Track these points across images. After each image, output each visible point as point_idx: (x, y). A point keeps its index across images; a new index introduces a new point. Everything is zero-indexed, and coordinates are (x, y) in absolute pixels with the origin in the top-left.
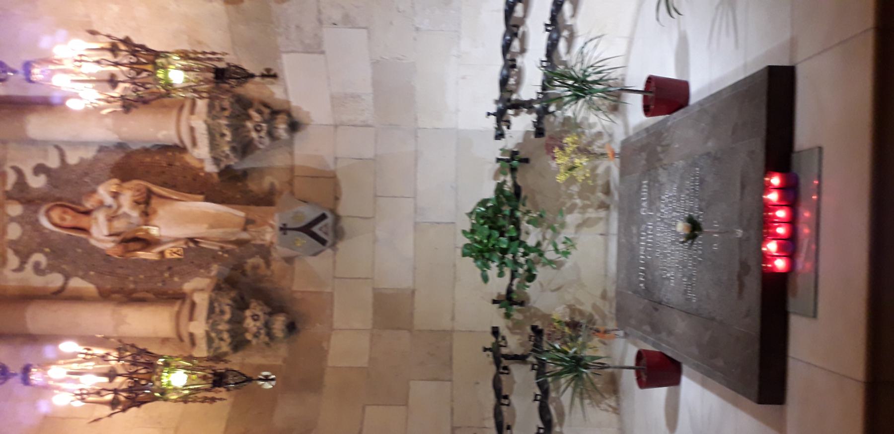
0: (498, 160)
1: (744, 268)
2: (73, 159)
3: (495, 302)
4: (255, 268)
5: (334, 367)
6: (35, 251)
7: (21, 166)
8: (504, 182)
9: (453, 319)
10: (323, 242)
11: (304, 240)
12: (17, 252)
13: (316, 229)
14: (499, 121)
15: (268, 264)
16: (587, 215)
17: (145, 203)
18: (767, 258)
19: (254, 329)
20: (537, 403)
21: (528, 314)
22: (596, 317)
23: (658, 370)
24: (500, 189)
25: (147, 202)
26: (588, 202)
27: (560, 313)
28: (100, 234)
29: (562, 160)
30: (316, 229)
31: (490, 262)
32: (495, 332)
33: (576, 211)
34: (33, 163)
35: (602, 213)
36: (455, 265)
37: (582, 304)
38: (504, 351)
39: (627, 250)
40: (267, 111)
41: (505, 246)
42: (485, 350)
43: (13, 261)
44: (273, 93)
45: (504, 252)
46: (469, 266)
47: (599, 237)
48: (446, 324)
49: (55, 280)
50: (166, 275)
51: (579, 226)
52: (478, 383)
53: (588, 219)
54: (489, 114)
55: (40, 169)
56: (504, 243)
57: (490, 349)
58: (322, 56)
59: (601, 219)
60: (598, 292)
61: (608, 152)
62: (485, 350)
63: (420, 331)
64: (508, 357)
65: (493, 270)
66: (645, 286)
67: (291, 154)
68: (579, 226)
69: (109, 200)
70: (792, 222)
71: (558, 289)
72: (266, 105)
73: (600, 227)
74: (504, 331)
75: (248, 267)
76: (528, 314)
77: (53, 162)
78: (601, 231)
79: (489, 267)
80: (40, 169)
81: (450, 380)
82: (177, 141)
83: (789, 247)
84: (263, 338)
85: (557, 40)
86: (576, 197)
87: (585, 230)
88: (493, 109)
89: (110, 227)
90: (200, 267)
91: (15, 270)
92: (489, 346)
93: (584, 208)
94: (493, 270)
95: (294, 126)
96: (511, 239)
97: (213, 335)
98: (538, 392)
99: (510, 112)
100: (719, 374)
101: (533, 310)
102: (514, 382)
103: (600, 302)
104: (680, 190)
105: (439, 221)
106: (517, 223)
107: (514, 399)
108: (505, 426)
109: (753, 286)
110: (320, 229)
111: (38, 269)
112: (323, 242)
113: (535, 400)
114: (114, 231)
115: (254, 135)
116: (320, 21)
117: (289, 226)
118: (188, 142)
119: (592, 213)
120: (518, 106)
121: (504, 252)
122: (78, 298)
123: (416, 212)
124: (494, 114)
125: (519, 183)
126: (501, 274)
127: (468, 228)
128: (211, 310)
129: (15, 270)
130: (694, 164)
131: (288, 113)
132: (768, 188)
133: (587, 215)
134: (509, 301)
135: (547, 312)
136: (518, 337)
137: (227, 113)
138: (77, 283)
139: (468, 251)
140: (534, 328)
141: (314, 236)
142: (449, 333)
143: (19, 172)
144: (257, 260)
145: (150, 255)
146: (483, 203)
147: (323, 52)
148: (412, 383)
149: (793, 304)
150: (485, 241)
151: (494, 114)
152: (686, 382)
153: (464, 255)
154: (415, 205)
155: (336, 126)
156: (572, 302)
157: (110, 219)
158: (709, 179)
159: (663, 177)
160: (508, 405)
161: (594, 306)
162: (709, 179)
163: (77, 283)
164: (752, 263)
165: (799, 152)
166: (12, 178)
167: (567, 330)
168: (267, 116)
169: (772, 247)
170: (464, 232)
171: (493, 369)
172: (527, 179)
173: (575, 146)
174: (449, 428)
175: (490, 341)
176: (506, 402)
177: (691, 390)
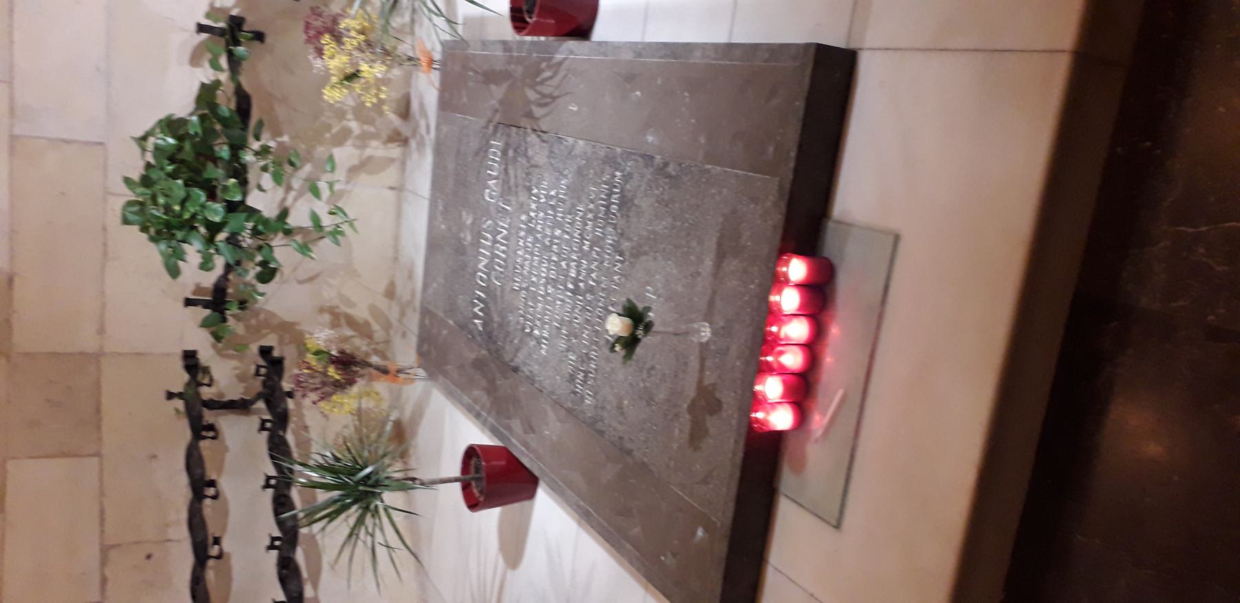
0: (201, 28)
1: (706, 403)
3: (189, 302)
8: (217, 84)
9: (101, 331)
16: (368, 152)
18: (758, 401)
21: (253, 322)
22: (376, 327)
23: (496, 479)
24: (207, 94)
26: (372, 129)
27: (321, 336)
29: (336, 61)
31: (185, 246)
32: (191, 360)
33: (349, 142)
35: (395, 151)
36: (104, 229)
37: (352, 305)
38: (206, 393)
39: (448, 248)
41: (217, 219)
45: (214, 228)
46: (140, 251)
47: (390, 194)
48: (87, 341)
51: (354, 171)
52: (154, 457)
53: (370, 158)
56: (216, 212)
57: (180, 395)
59: (392, 160)
60: (382, 286)
61: (419, 54)
63: (27, 354)
64: (212, 405)
65: (193, 252)
66: (484, 325)
68: (354, 171)
70: (812, 348)
71: (311, 279)
73: (390, 175)
74: (206, 355)
76: (253, 322)
78: (392, 181)
79: (180, 255)
81: (98, 454)
83: (801, 390)
86: (350, 116)
87: (363, 177)
92: (178, 388)
93: (364, 139)
94: (193, 252)
96: (232, 207)
100: (628, 546)
101: (262, 316)
102: (226, 449)
103: (382, 303)
104: (576, 192)
105: (66, 136)
106: (240, 173)
107: (226, 484)
108: (211, 540)
109: (725, 448)
113: (267, 486)
119: (376, 149)
121: (214, 228)
123: (12, 111)
125: (247, 87)
126: (206, 265)
127: (136, 176)
130: (611, 162)
132: (780, 282)
133: (368, 152)
134: (217, 303)
135: (288, 317)
136: (234, 363)
139: (137, 214)
140: (265, 352)
142: (96, 357)
146: (171, 125)
148: (10, 465)
149: (787, 480)
150: (177, 208)
152: (544, 500)
153: (126, 222)
154: (12, 99)
156: (336, 302)
158: (645, 203)
159: (538, 152)
160: (215, 497)
161: (373, 310)
162: (645, 203)
164: (728, 398)
165: (839, 222)
167: (332, 371)
169: (772, 387)
170: (127, 181)
171: (185, 433)
172: (261, 72)
173: (362, 37)
174: (95, 552)
175: (179, 379)
177: (548, 513)
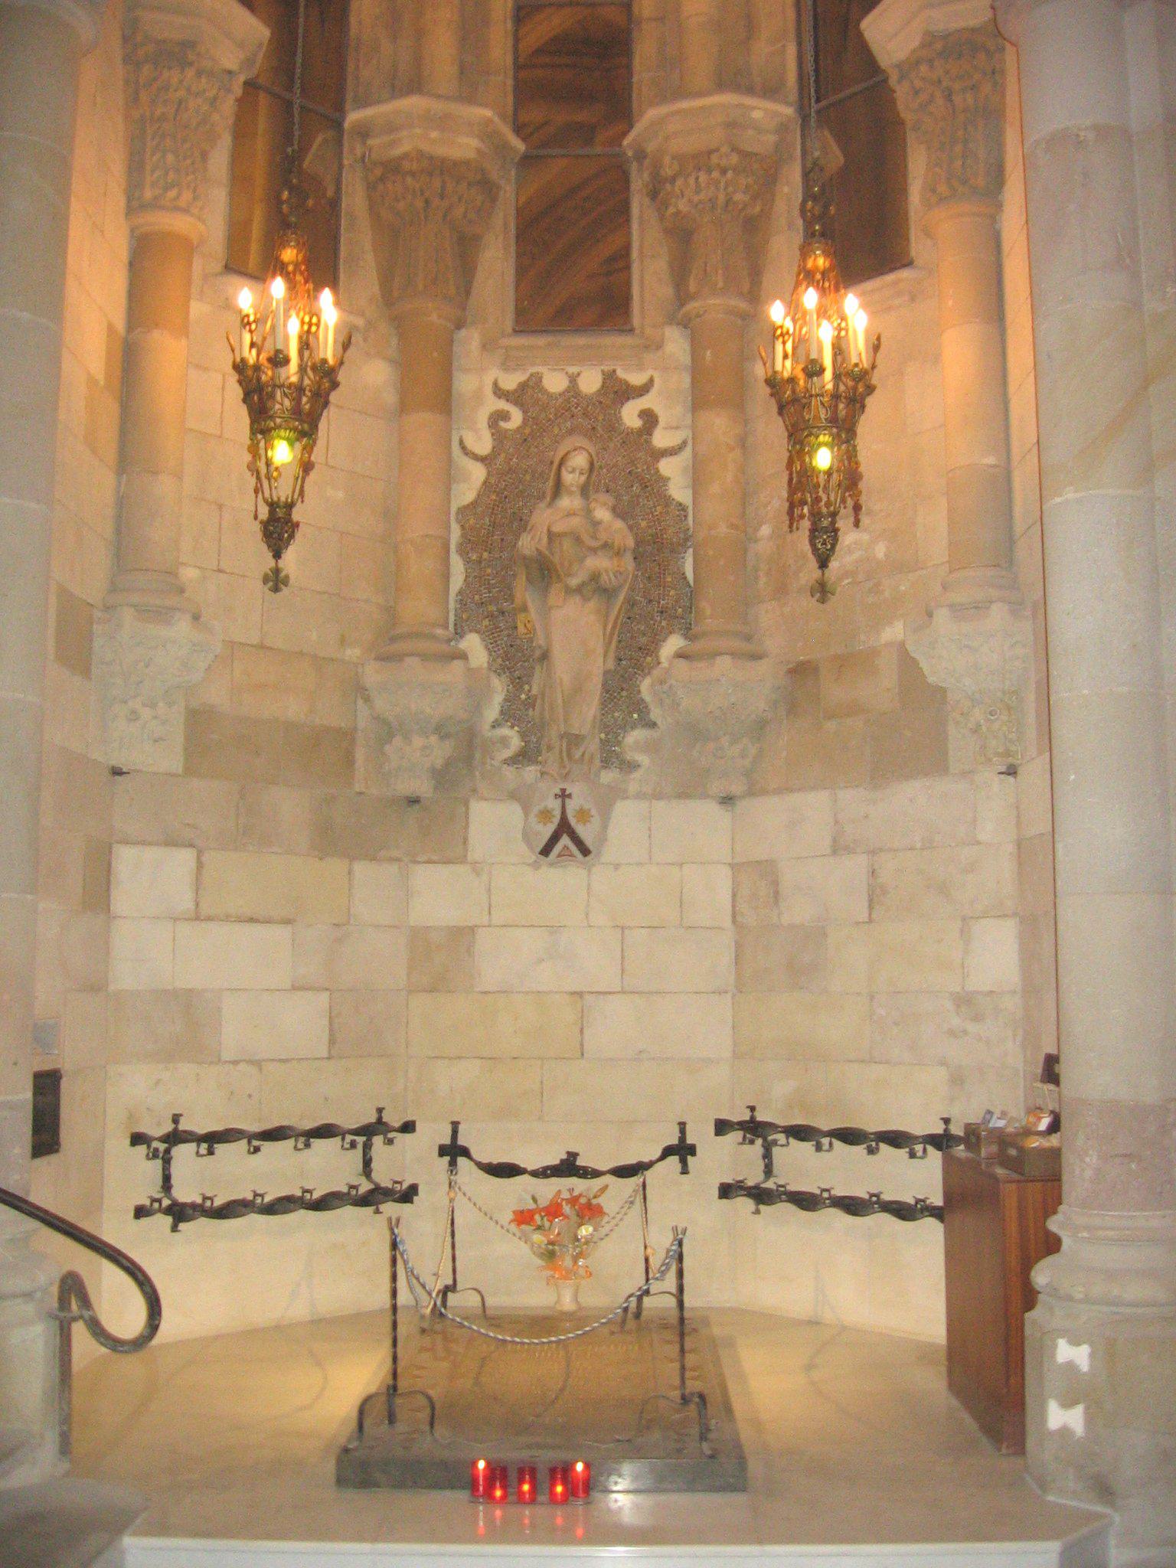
6: (525, 412)
12: (523, 386)
13: (565, 840)
17: (597, 588)
20: (867, 1197)
30: (565, 840)
34: (658, 410)
42: (380, 1110)
43: (511, 382)
50: (492, 608)
54: (752, 1109)
55: (650, 419)
58: (829, 851)
64: (367, 1147)
77: (661, 439)
80: (650, 419)
90: (506, 657)
98: (267, 1199)
110: (566, 847)
117: (567, 801)
124: (752, 1117)
129: (495, 384)
141: (554, 839)
147: (834, 852)
151: (752, 1117)
166: (636, 379)
176: (300, 1145)
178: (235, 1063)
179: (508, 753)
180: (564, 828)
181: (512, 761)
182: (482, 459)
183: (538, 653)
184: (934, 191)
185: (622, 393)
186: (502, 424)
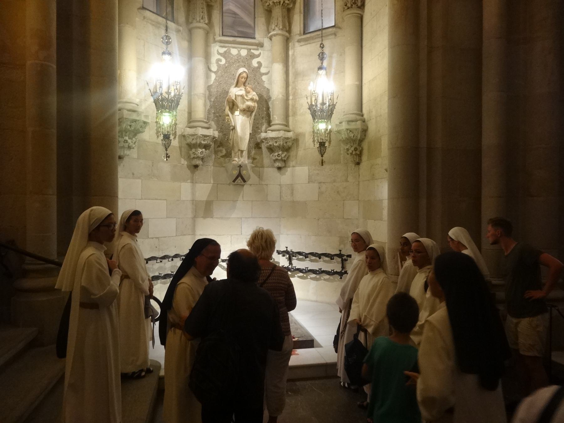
2: (264, 78)
4: (221, 151)
5: (180, 186)
6: (226, 60)
7: (261, 56)
10: (234, 181)
11: (236, 173)
12: (225, 52)
13: (240, 178)
14: (284, 251)
15: (222, 157)
19: (197, 153)
25: (248, 111)
28: (235, 92)
30: (240, 178)
40: (285, 159)
43: (222, 50)
44: (293, 161)
49: (214, 68)
54: (287, 248)
62: (341, 278)
67: (268, 167)
69: (250, 96)
72: (288, 158)
75: (221, 148)
77: (263, 70)
80: (260, 64)
82: (273, 123)
84: (192, 156)
85: (303, 273)
88: (289, 249)
89: (238, 96)
90: (221, 129)
91: (218, 51)
95: (279, 168)
97: (195, 137)
99: (288, 256)
111: (218, 60)
112: (234, 181)
114: (237, 97)
115: (276, 154)
116: (320, 183)
118: (273, 128)
120: (290, 260)
122: (208, 77)
128: (205, 136)
129: (218, 51)
131: (285, 167)
137: (285, 144)
138: (213, 76)
143: (258, 56)
144: (224, 152)
145: (227, 111)
147: (309, 183)
155: (280, 185)
157: (242, 96)
163: (213, 76)
166: (256, 52)
168: (283, 159)
178: (152, 238)
179: (221, 154)
180: (240, 175)
181: (222, 157)
182: (215, 72)
183: (232, 128)
184: (346, 5)
185: (253, 56)
186: (219, 62)
